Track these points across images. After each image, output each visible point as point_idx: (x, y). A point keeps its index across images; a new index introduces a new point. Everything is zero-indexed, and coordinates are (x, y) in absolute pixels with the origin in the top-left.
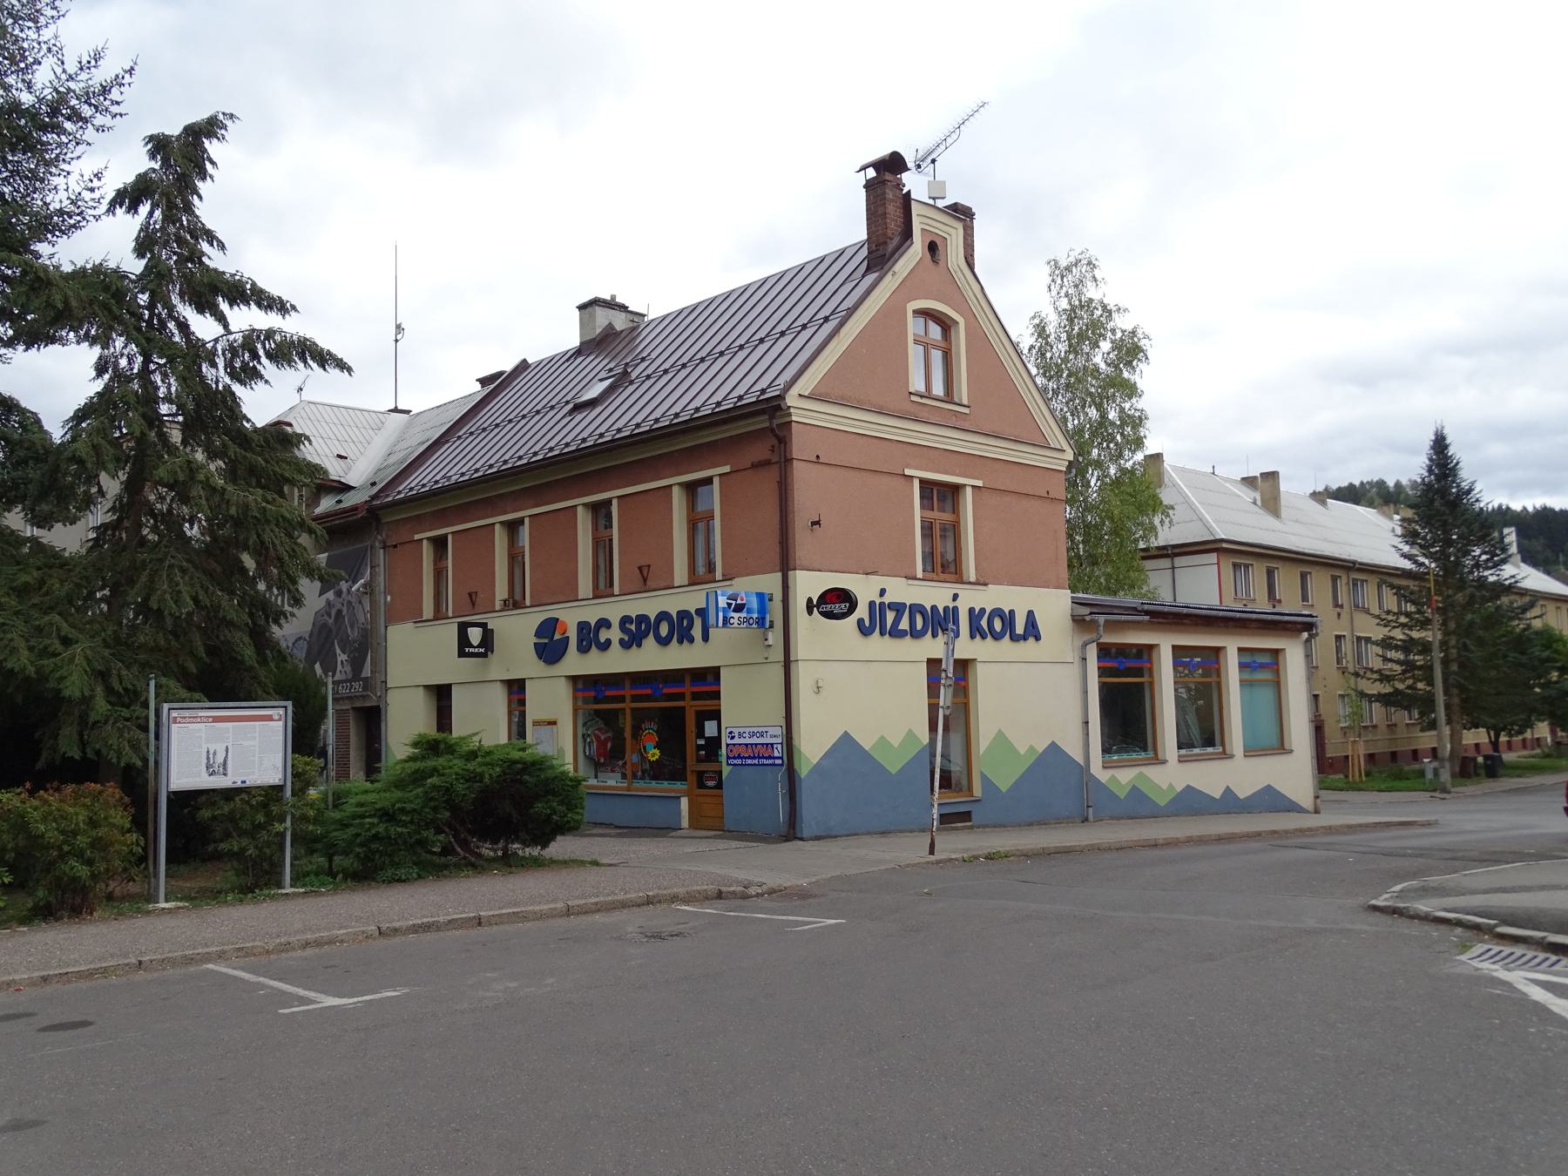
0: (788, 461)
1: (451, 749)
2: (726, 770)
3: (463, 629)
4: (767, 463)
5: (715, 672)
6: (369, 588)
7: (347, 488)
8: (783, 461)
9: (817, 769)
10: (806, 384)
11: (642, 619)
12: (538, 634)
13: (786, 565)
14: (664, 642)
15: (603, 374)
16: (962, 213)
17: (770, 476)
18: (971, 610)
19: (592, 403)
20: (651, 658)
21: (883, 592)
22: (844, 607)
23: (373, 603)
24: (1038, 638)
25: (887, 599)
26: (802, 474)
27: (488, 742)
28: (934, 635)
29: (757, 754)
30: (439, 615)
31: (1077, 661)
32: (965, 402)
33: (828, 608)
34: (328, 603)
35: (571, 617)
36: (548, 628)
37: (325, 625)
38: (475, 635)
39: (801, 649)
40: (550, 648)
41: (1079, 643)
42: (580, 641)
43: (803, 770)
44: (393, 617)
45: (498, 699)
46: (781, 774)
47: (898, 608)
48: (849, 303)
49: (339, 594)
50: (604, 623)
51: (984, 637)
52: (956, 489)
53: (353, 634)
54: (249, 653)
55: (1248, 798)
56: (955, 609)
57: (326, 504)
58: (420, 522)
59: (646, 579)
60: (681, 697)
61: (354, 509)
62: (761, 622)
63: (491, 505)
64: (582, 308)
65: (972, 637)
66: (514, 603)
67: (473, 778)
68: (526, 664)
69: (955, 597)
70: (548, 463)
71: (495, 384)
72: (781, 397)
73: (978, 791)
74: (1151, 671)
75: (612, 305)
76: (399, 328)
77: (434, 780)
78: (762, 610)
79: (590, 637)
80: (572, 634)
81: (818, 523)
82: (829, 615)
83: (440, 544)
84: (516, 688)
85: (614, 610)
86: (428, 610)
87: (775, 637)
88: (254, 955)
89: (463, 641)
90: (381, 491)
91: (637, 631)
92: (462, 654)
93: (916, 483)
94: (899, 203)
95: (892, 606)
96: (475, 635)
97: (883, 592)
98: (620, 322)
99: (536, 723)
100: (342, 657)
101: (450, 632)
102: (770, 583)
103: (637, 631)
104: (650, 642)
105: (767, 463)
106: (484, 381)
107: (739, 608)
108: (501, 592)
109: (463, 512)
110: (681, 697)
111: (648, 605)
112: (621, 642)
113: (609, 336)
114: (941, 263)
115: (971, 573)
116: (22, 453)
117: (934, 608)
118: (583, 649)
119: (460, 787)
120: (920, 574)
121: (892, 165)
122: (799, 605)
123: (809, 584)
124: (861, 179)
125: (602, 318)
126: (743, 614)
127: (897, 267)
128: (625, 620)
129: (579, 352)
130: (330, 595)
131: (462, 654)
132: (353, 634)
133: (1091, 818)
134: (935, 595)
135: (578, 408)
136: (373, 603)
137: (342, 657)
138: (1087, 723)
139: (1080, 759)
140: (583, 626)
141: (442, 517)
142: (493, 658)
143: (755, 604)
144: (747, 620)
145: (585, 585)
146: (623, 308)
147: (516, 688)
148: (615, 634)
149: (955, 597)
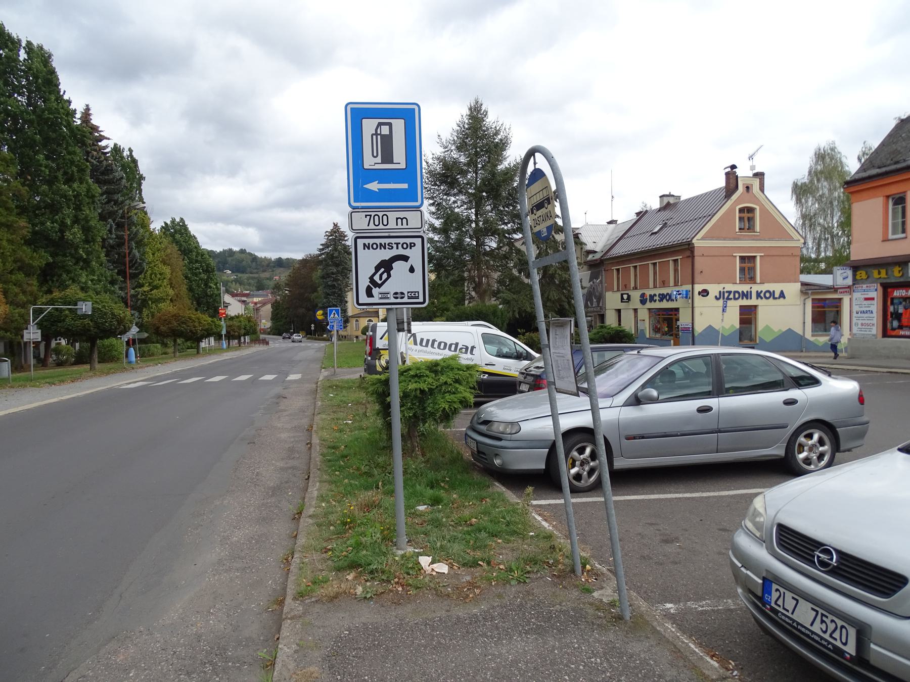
0: (693, 257)
1: (605, 327)
2: (680, 334)
3: (622, 295)
4: (689, 257)
5: (678, 309)
6: (601, 281)
7: (595, 252)
8: (693, 257)
9: (700, 334)
10: (699, 236)
11: (663, 294)
12: (641, 297)
13: (693, 283)
14: (668, 301)
15: (660, 223)
16: (760, 176)
17: (690, 259)
18: (757, 292)
19: (656, 233)
20: (665, 305)
21: (724, 288)
22: (706, 294)
23: (602, 286)
24: (784, 298)
25: (725, 290)
26: (698, 260)
27: (612, 326)
28: (743, 299)
29: (686, 330)
30: (618, 290)
31: (802, 304)
32: (758, 231)
33: (702, 294)
34: (591, 285)
35: (648, 293)
36: (643, 295)
37: (590, 291)
38: (625, 297)
39: (696, 304)
40: (643, 302)
41: (803, 298)
42: (650, 299)
43: (696, 334)
44: (607, 290)
45: (632, 313)
46: (691, 335)
47: (730, 292)
48: (714, 212)
49: (594, 283)
50: (655, 295)
51: (762, 298)
52: (755, 257)
53: (597, 294)
54: (567, 307)
55: (770, 342)
56: (751, 292)
57: (590, 257)
58: (613, 264)
59: (664, 284)
60: (671, 315)
61: (596, 260)
62: (686, 297)
63: (630, 261)
64: (660, 197)
65: (757, 298)
66: (635, 288)
67: (609, 333)
68: (638, 305)
69: (751, 288)
70: (642, 252)
71: (641, 215)
72: (691, 241)
73: (758, 342)
74: (840, 306)
75: (670, 195)
76: (613, 197)
77: (601, 333)
78: (687, 295)
79: (652, 298)
80: (648, 297)
81: (701, 272)
82: (703, 296)
83: (618, 270)
84: (636, 310)
85: (658, 291)
86: (615, 289)
87: (690, 301)
88: (675, 646)
89: (622, 298)
90: (605, 254)
91: (663, 297)
92: (622, 302)
93: (738, 258)
94: (735, 178)
95: (727, 292)
96: (625, 297)
97: (724, 288)
98: (672, 201)
99: (640, 320)
100: (595, 300)
101: (618, 295)
102: (689, 287)
103: (663, 297)
104: (665, 300)
105: (689, 257)
106: (638, 214)
107: (680, 294)
108: (632, 285)
109: (623, 262)
110: (671, 315)
111: (664, 291)
112: (659, 300)
113: (668, 204)
114: (750, 192)
115: (758, 280)
116: (523, 262)
117: (743, 292)
118: (651, 301)
119: (606, 335)
120: (738, 282)
121: (733, 167)
122: (696, 293)
123: (698, 288)
124: (724, 172)
125: (666, 200)
126: (681, 296)
127: (732, 198)
128: (659, 295)
129: (660, 210)
130: (591, 283)
131: (622, 302)
132: (597, 294)
133: (804, 350)
134: (745, 288)
135: (652, 234)
136: (602, 286)
137: (595, 300)
138: (804, 323)
139: (801, 333)
140: (650, 296)
141: (618, 263)
142: (630, 302)
143: (684, 293)
144: (682, 297)
145: (651, 284)
146: (673, 196)
147: (636, 310)
148: (657, 298)
149: (751, 288)
